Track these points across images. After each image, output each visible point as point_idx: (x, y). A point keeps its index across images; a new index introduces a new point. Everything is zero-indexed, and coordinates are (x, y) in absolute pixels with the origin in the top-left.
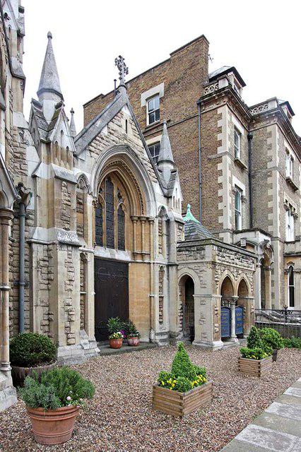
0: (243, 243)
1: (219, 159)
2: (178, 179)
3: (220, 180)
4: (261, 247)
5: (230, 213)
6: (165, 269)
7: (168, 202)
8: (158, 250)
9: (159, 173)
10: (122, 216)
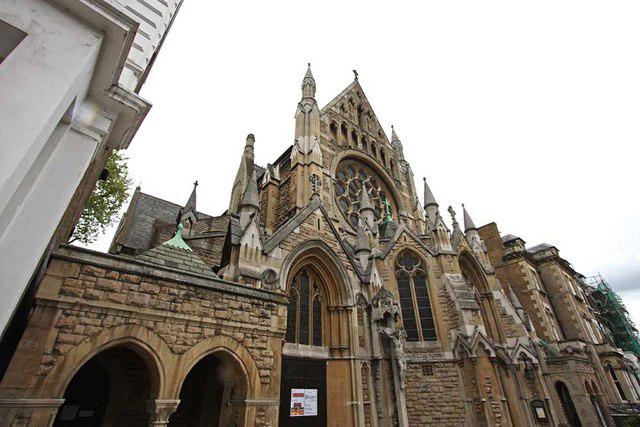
0: (570, 350)
1: (531, 293)
3: (536, 306)
10: (317, 310)
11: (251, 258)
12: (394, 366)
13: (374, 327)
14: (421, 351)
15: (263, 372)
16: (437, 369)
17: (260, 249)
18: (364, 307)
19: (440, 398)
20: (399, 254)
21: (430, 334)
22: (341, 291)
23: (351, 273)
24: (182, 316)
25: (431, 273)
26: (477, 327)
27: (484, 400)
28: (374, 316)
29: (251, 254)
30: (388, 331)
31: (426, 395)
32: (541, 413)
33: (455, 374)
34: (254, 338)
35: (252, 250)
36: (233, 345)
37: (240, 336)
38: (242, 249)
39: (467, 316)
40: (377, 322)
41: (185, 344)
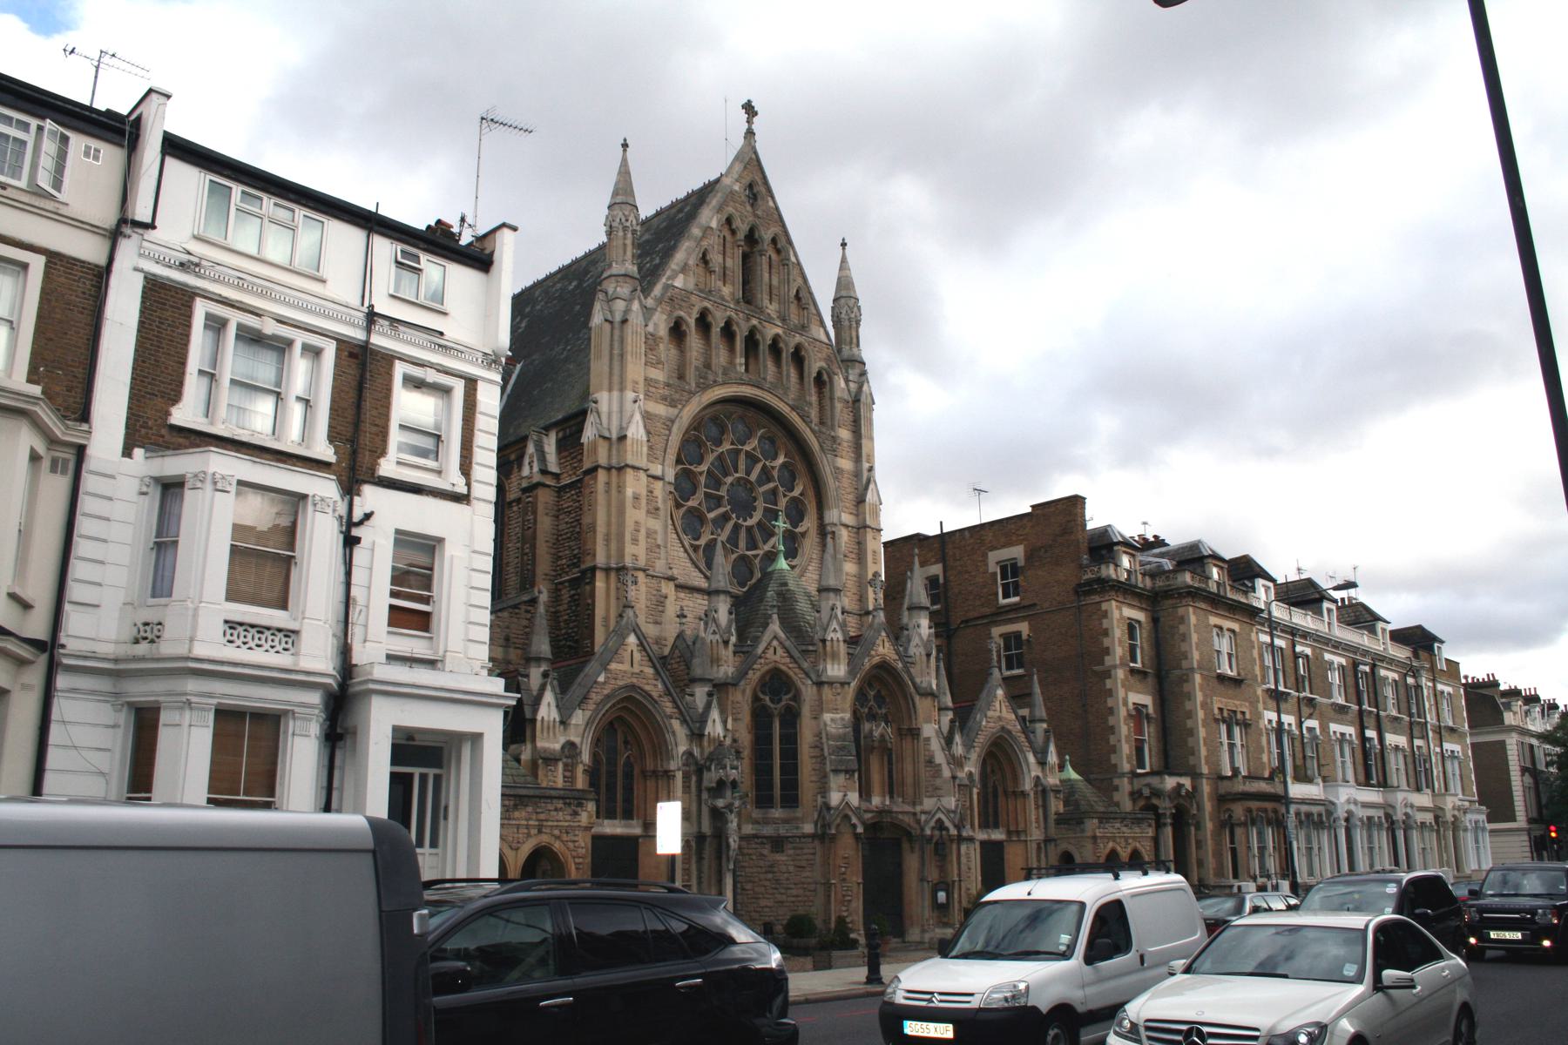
2: (1052, 739)
4: (1169, 797)
5: (1126, 749)
6: (1043, 845)
7: (1043, 768)
8: (1034, 825)
9: (1032, 735)
10: (629, 776)
11: (548, 732)
12: (724, 844)
13: (705, 795)
14: (774, 821)
15: (577, 860)
16: (790, 846)
17: (558, 720)
18: (693, 768)
19: (788, 879)
20: (763, 677)
21: (791, 798)
22: (661, 748)
23: (676, 724)
24: (514, 822)
25: (806, 711)
26: (845, 795)
27: (833, 881)
28: (705, 784)
29: (549, 728)
30: (720, 803)
31: (770, 876)
32: (942, 896)
33: (812, 851)
34: (567, 833)
35: (549, 722)
36: (552, 840)
37: (556, 832)
38: (539, 725)
39: (836, 781)
40: (709, 790)
41: (518, 842)
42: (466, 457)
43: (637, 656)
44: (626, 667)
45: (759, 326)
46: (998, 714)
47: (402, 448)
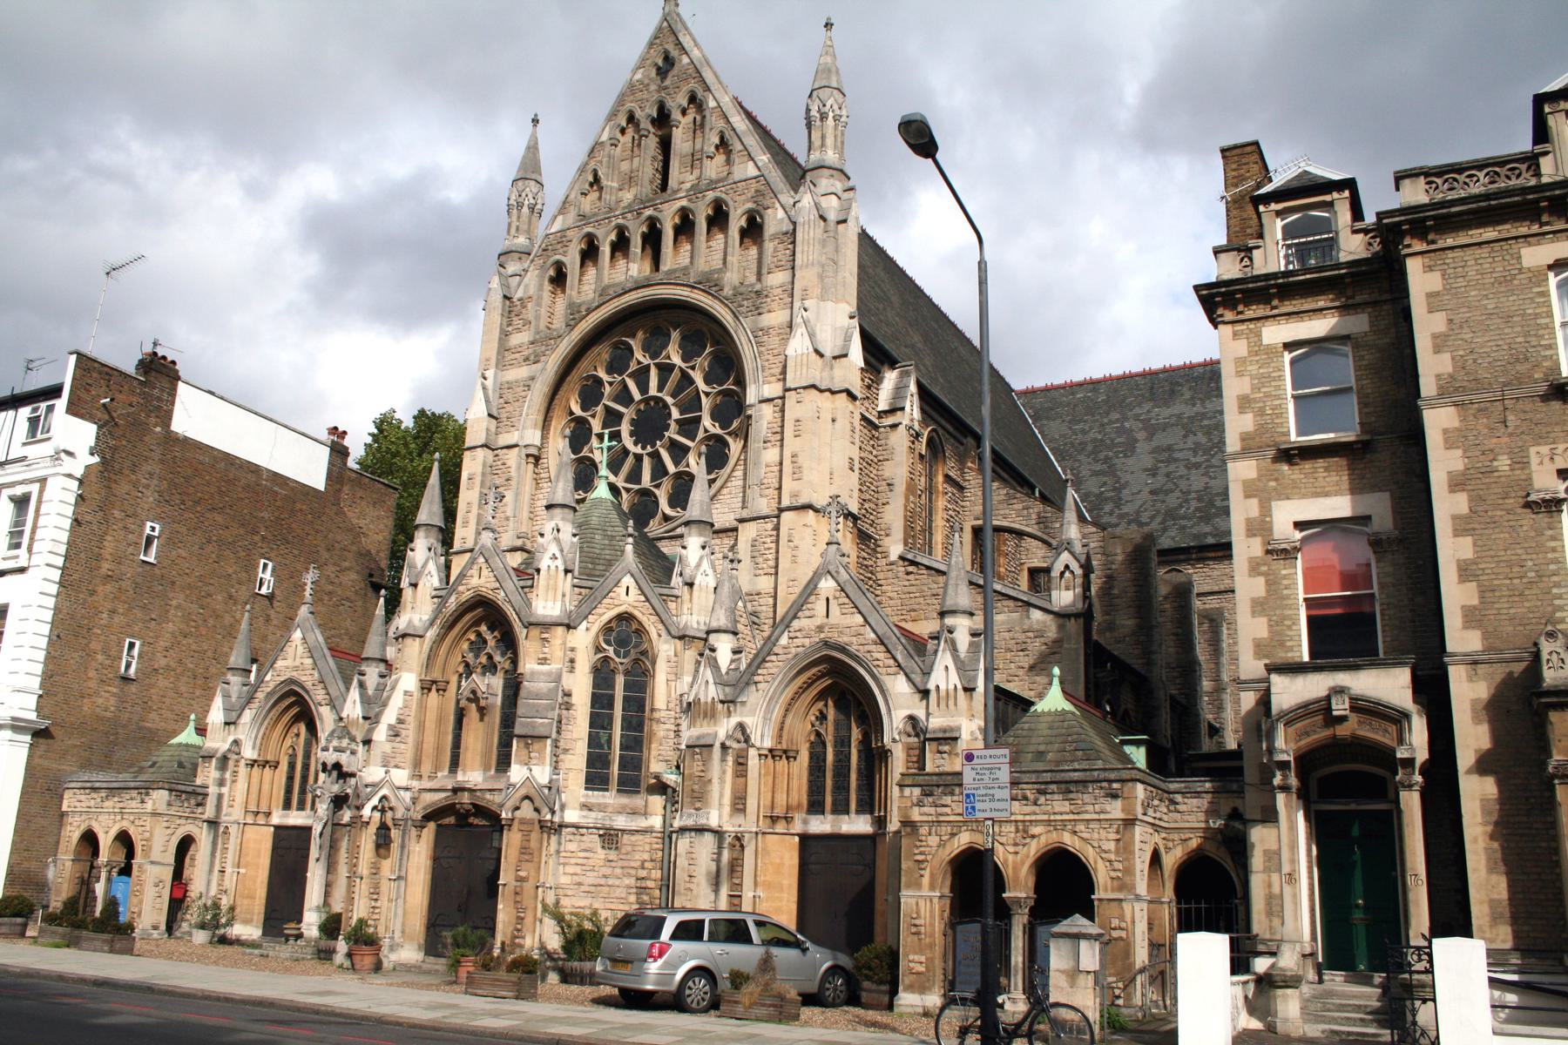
17: (959, 687)
42: (450, 492)
43: (300, 649)
44: (289, 663)
45: (656, 214)
46: (818, 621)
47: (145, 555)
